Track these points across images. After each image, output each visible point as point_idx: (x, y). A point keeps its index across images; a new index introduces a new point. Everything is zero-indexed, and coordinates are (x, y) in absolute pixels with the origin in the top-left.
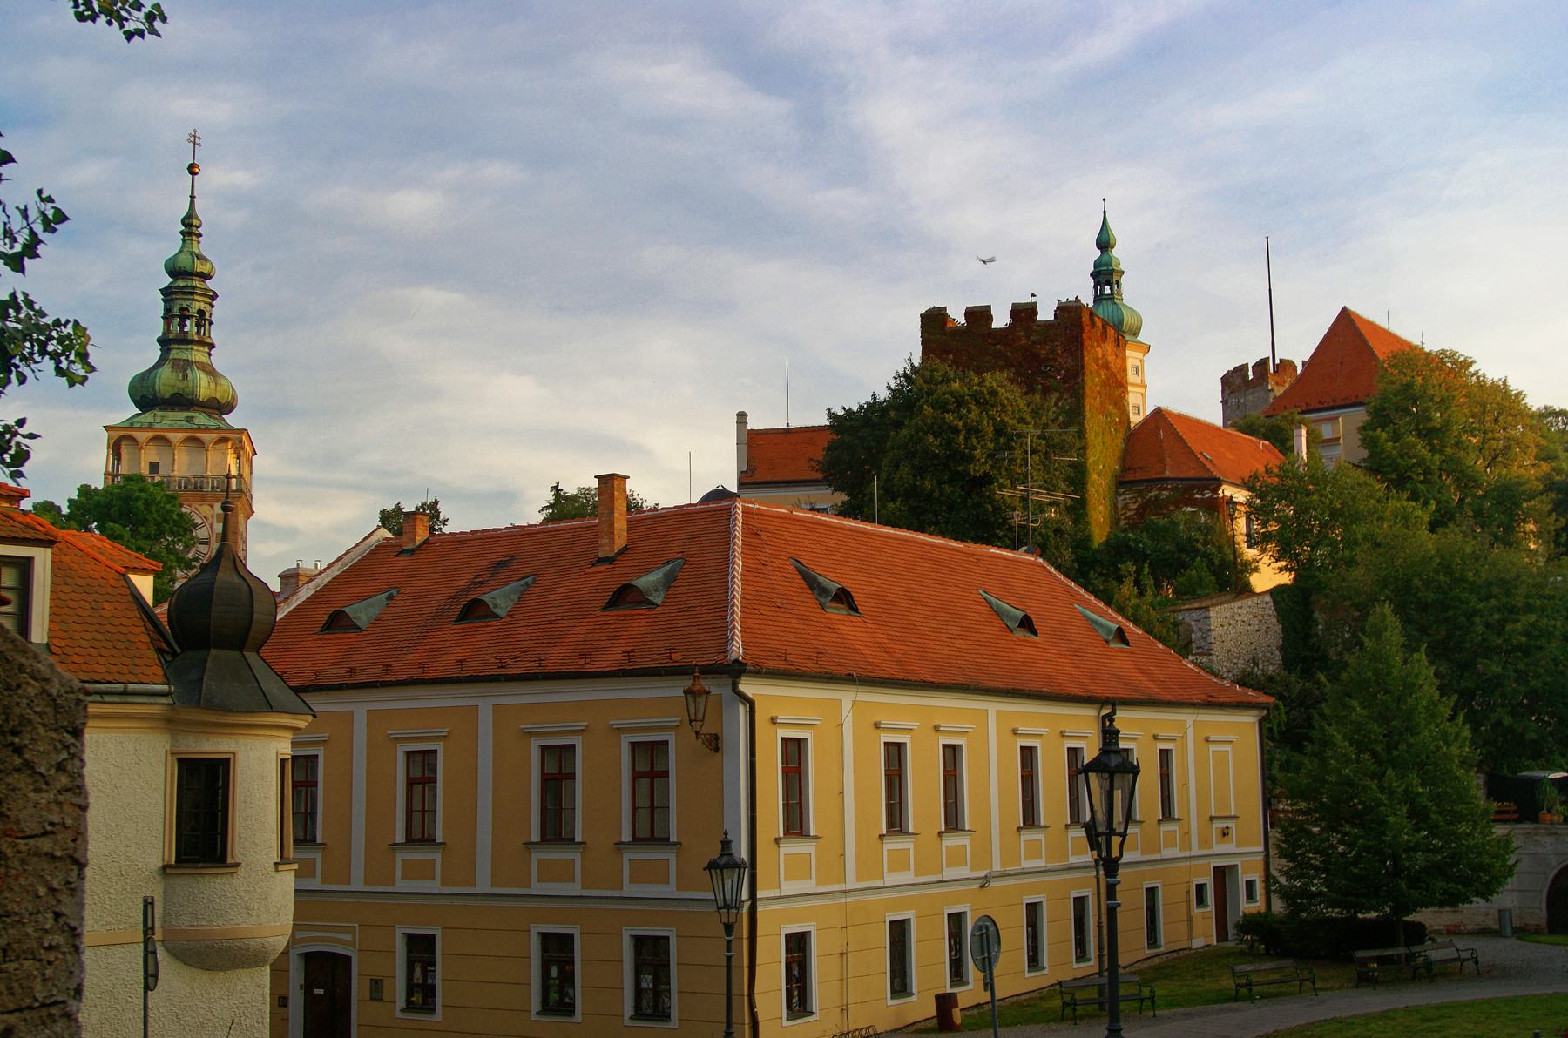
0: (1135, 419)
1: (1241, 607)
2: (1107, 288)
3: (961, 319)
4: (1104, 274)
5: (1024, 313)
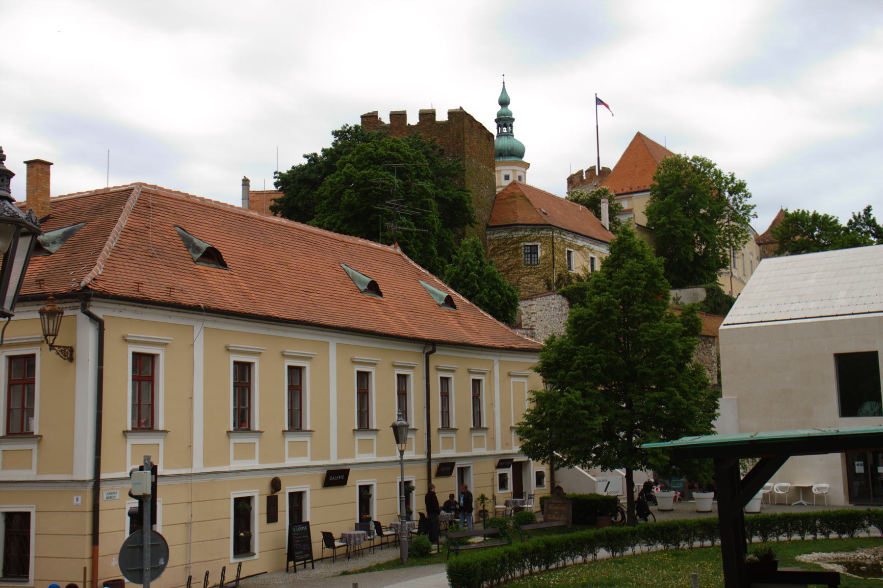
0: (498, 190)
1: (554, 299)
2: (505, 128)
3: (386, 120)
4: (503, 120)
5: (427, 116)
